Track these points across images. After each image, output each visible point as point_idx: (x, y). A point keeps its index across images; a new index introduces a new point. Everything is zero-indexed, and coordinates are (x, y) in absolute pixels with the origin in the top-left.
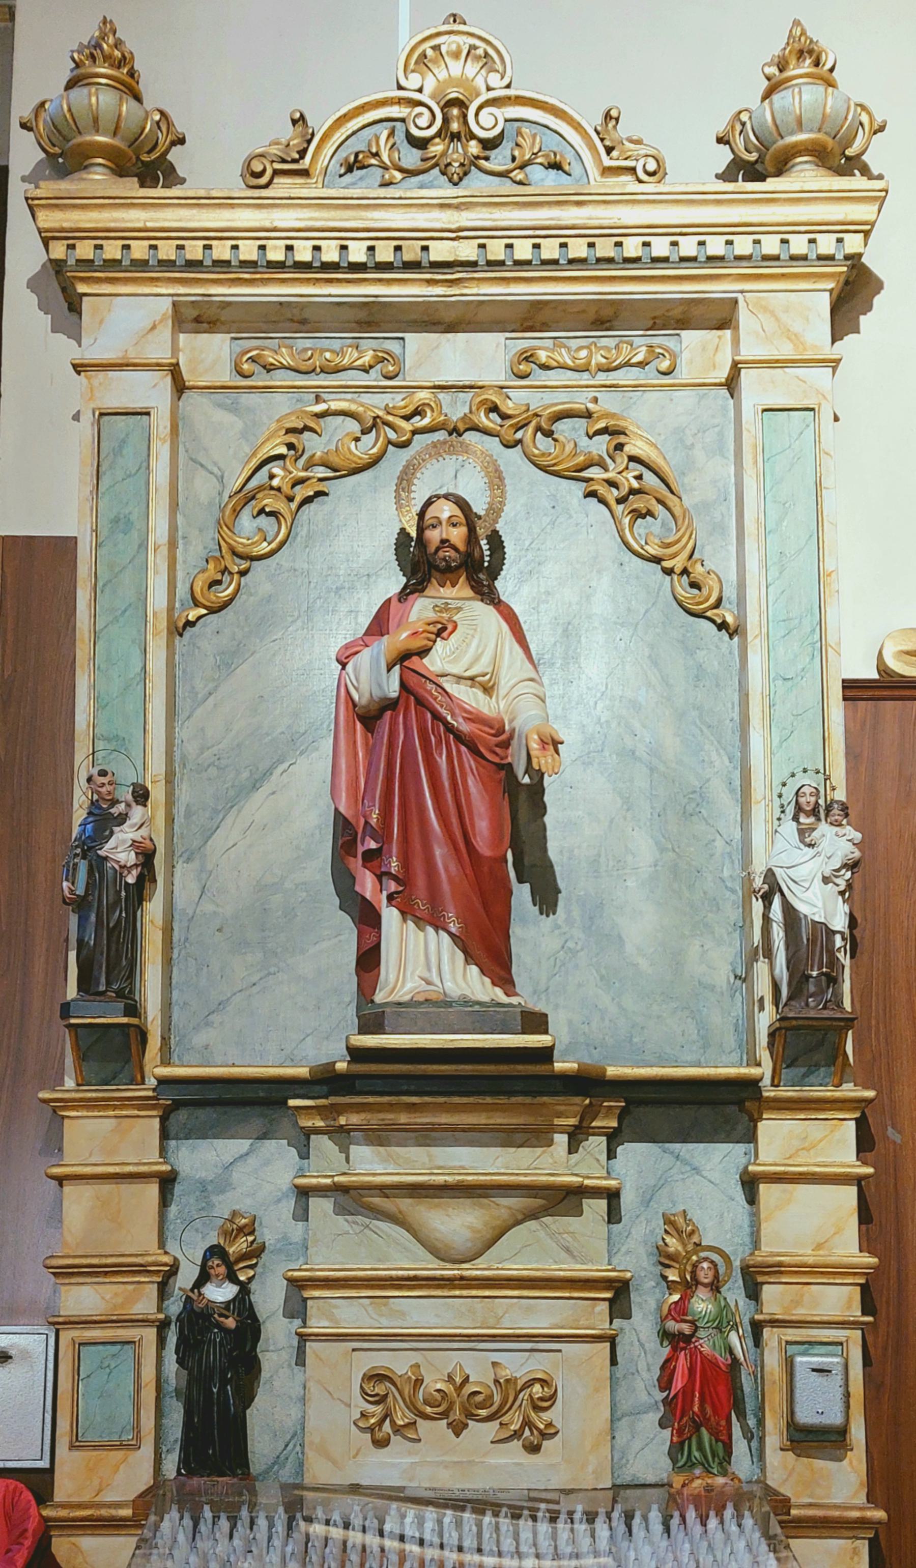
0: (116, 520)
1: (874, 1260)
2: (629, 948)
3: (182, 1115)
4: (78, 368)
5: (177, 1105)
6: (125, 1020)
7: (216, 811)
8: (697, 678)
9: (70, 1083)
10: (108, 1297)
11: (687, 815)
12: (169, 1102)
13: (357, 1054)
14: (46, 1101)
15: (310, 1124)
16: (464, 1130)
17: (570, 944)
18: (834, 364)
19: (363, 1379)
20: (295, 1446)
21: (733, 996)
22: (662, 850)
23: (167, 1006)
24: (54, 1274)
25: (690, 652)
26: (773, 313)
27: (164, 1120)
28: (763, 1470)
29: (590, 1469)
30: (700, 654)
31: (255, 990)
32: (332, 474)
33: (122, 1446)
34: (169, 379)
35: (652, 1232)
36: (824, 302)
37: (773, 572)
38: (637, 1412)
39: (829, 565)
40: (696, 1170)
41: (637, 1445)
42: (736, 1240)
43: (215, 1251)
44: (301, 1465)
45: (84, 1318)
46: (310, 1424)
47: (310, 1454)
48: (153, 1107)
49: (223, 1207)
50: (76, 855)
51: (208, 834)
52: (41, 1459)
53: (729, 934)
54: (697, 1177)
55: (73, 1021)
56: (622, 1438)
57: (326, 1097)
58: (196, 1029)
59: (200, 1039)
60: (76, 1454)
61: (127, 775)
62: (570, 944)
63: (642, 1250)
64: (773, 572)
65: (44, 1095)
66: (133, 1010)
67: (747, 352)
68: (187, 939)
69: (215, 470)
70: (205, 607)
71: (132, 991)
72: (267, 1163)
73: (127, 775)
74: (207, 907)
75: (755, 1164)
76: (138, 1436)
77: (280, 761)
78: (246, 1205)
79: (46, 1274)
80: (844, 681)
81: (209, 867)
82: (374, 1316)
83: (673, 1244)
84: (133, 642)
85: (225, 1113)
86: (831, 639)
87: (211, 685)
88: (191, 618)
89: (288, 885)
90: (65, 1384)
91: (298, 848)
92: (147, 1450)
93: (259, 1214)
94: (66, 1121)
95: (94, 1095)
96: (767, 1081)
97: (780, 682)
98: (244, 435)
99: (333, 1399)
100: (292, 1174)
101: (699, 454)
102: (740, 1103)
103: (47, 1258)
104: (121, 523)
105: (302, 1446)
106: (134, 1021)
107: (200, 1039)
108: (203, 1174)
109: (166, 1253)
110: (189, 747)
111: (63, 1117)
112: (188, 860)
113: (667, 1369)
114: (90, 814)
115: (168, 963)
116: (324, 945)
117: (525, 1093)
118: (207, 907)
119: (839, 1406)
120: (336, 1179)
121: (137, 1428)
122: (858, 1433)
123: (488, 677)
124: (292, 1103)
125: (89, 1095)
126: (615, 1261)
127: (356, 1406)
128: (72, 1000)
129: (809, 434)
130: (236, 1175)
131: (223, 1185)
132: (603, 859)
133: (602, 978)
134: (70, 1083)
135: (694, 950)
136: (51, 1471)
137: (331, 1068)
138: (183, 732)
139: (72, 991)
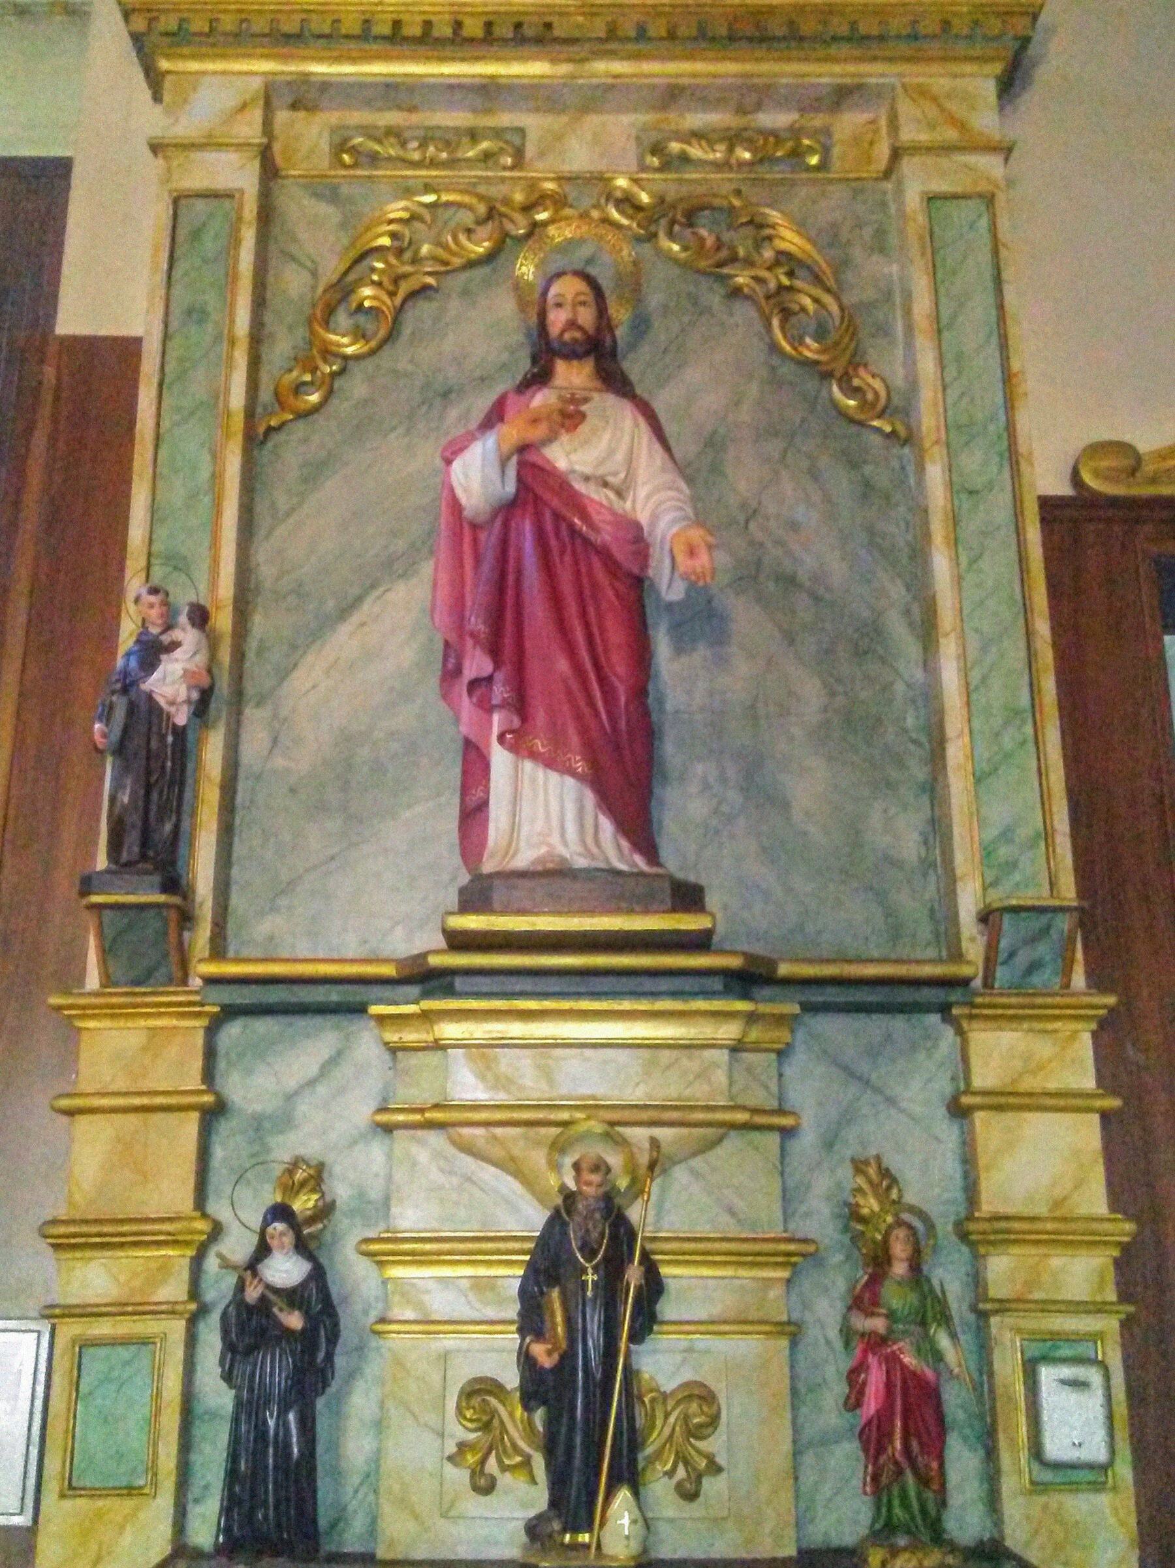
0: (189, 312)
1: (1129, 1227)
2: (797, 815)
3: (233, 1030)
4: (156, 148)
5: (230, 1012)
6: (162, 898)
7: (294, 647)
8: (865, 496)
9: (93, 981)
10: (122, 1278)
11: (860, 654)
12: (216, 1009)
13: (459, 941)
14: (59, 1008)
15: (395, 1038)
16: (594, 1046)
17: (725, 808)
18: (1007, 151)
19: (459, 1397)
20: (366, 1495)
21: (925, 875)
22: (833, 694)
23: (223, 887)
24: (53, 1245)
25: (854, 465)
26: (934, 99)
27: (212, 1031)
28: (998, 1523)
29: (768, 1527)
30: (868, 470)
31: (333, 865)
32: (443, 269)
33: (131, 1491)
34: (257, 164)
35: (839, 1185)
36: (989, 89)
37: (951, 372)
38: (826, 1441)
39: (1015, 365)
40: (891, 1101)
41: (827, 1490)
42: (946, 1196)
43: (281, 1212)
44: (374, 1521)
45: (89, 1310)
46: (388, 1464)
47: (387, 1509)
48: (198, 1015)
49: (284, 1149)
50: (113, 692)
51: (284, 673)
52: (21, 1513)
53: (916, 796)
54: (893, 1111)
55: (96, 899)
56: (809, 1477)
57: (416, 1002)
58: (262, 914)
59: (264, 927)
60: (68, 1504)
61: (183, 597)
62: (725, 808)
63: (826, 1210)
64: (951, 372)
65: (54, 1000)
66: (174, 883)
67: (909, 134)
68: (252, 802)
69: (309, 264)
70: (292, 412)
71: (173, 863)
72: (342, 1090)
73: (183, 597)
74: (279, 762)
75: (966, 1092)
76: (155, 1484)
77: (373, 586)
78: (312, 1149)
79: (43, 1246)
80: (1039, 497)
81: (284, 712)
82: (478, 1306)
83: (870, 1204)
84: (202, 445)
85: (291, 1025)
86: (1023, 448)
87: (295, 500)
88: (273, 423)
89: (378, 734)
90: (58, 1404)
91: (392, 689)
92: (165, 1502)
93: (329, 1159)
94: (84, 1033)
95: (122, 1000)
96: (977, 983)
97: (963, 496)
98: (343, 225)
99: (419, 1424)
100: (373, 1105)
101: (857, 253)
102: (944, 1009)
103: (45, 1223)
104: (196, 314)
105: (376, 1492)
106: (175, 900)
107: (264, 927)
108: (258, 1107)
109: (205, 1215)
110: (266, 571)
111: (80, 1029)
112: (258, 704)
113: (854, 1376)
114: (138, 641)
115: (227, 832)
116: (418, 809)
117: (675, 994)
118: (279, 762)
119: (1100, 1435)
120: (427, 1115)
121: (153, 1468)
122: (1124, 1471)
123: (622, 475)
124: (375, 1009)
125: (114, 1000)
126: (792, 1226)
127: (452, 1436)
128: (101, 873)
129: (984, 222)
130: (303, 1107)
131: (284, 1120)
132: (760, 705)
133: (764, 850)
134: (93, 981)
135: (876, 818)
136: (32, 1531)
137: (420, 961)
138: (262, 554)
139: (102, 862)
